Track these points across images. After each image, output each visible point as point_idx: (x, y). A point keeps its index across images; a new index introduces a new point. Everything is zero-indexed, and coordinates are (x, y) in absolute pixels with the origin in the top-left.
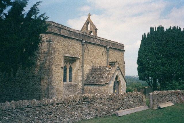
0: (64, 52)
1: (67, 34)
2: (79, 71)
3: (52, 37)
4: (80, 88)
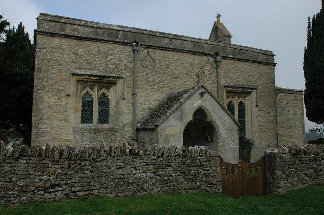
0: (75, 65)
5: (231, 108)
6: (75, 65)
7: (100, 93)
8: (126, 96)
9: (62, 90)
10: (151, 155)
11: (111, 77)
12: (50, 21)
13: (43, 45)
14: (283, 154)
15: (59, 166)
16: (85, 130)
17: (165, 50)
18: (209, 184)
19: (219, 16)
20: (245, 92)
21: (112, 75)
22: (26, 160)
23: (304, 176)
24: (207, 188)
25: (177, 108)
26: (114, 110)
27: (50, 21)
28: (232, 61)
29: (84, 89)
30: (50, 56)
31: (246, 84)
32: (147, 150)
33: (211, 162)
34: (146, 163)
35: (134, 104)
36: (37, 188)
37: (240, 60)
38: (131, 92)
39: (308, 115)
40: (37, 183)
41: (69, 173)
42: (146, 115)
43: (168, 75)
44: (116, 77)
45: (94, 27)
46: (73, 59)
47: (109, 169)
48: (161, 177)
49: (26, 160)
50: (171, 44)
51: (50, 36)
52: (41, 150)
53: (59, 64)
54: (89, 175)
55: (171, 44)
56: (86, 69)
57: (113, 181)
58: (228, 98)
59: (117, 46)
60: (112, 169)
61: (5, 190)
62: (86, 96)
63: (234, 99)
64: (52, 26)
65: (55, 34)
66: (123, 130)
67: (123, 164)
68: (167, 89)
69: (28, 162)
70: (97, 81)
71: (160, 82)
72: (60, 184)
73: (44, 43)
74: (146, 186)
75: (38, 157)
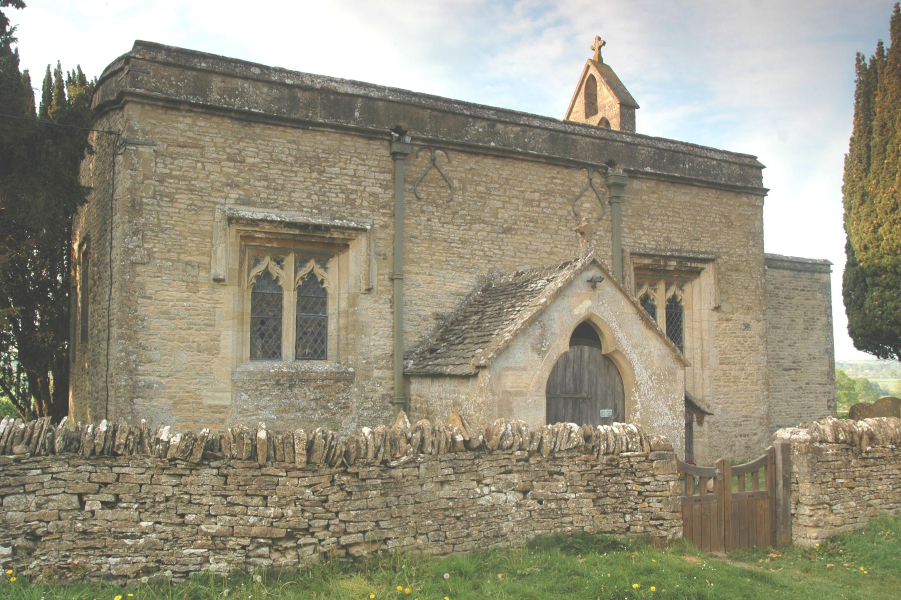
0: (234, 195)
1: (258, 98)
2: (366, 303)
3: (103, 124)
4: (377, 396)
5: (647, 307)
6: (234, 195)
7: (303, 272)
8: (375, 283)
9: (200, 266)
10: (514, 449)
11: (335, 227)
12: (166, 64)
13: (145, 133)
14: (821, 442)
15: (306, 482)
16: (265, 377)
17: (477, 154)
18: (651, 519)
19: (601, 44)
20: (687, 269)
21: (338, 222)
22: (218, 468)
23: (872, 496)
24: (649, 529)
25: (532, 321)
26: (342, 321)
27: (166, 64)
28: (651, 184)
29: (257, 261)
30: (166, 166)
31: (688, 247)
32: (504, 434)
33: (655, 464)
34: (503, 470)
35: (397, 305)
36: (253, 538)
37: (673, 181)
38: (388, 270)
39: (852, 332)
40: (252, 525)
41: (332, 498)
42: (426, 334)
43: (484, 222)
44: (349, 228)
45: (288, 86)
46: (228, 175)
47: (422, 485)
48: (540, 502)
49: (218, 468)
50: (494, 134)
51: (163, 107)
52: (254, 439)
53: (191, 190)
54: (378, 502)
55: (494, 134)
56: (265, 205)
57: (431, 515)
58: (639, 286)
59: (349, 141)
60: (429, 486)
61: (172, 547)
62: (264, 282)
63: (655, 290)
64: (166, 80)
65: (180, 102)
66: (367, 378)
67: (451, 471)
68: (482, 263)
69: (225, 472)
70: (298, 238)
71: (464, 242)
72: (310, 526)
73: (148, 128)
74: (505, 528)
75: (249, 459)
